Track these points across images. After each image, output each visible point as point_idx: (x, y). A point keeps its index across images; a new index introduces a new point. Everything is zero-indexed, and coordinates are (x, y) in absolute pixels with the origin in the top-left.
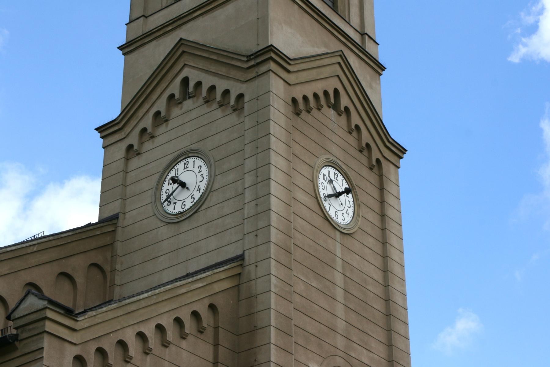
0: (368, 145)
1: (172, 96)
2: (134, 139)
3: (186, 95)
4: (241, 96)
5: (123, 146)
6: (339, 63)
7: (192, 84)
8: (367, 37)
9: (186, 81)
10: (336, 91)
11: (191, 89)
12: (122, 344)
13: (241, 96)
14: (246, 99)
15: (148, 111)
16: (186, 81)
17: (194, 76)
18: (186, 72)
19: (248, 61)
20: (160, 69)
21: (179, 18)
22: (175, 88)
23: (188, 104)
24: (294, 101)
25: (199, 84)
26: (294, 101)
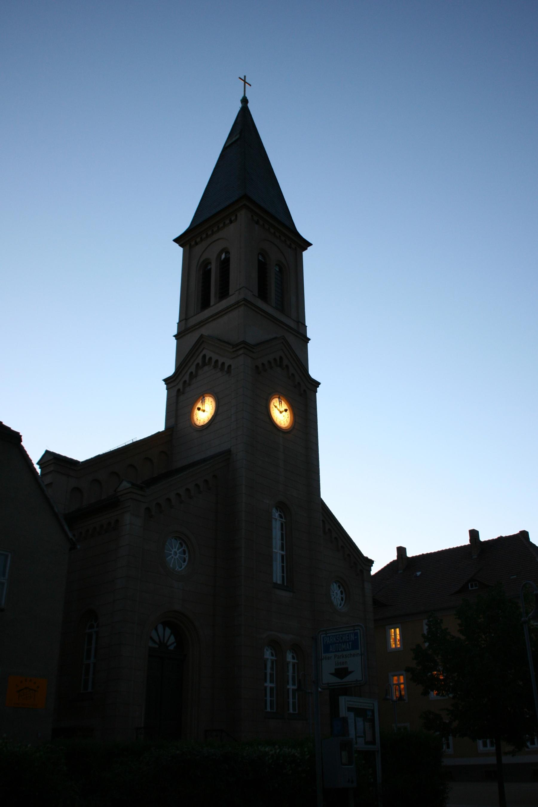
0: (299, 383)
1: (198, 364)
2: (180, 386)
3: (204, 364)
4: (230, 366)
5: (176, 389)
6: (283, 343)
7: (207, 358)
8: (300, 324)
9: (204, 356)
10: (281, 358)
11: (207, 361)
12: (169, 500)
13: (230, 366)
14: (232, 368)
15: (180, 380)
16: (204, 356)
17: (209, 354)
18: (204, 352)
19: (233, 348)
20: (220, 314)
21: (202, 322)
22: (199, 360)
23: (206, 368)
24: (257, 367)
25: (210, 359)
26: (257, 367)
